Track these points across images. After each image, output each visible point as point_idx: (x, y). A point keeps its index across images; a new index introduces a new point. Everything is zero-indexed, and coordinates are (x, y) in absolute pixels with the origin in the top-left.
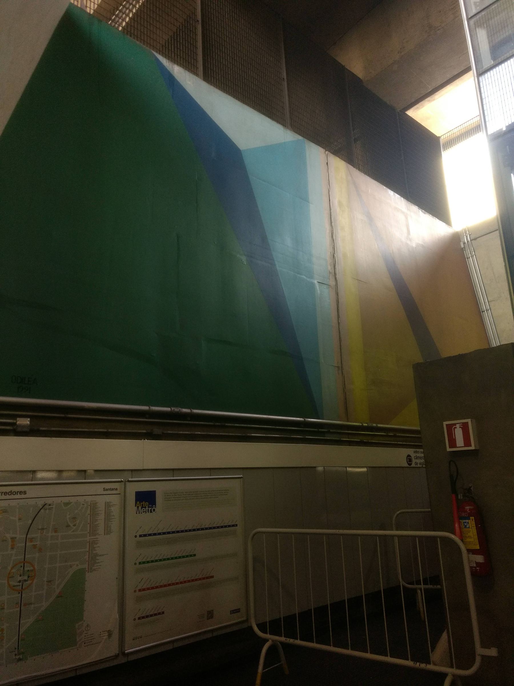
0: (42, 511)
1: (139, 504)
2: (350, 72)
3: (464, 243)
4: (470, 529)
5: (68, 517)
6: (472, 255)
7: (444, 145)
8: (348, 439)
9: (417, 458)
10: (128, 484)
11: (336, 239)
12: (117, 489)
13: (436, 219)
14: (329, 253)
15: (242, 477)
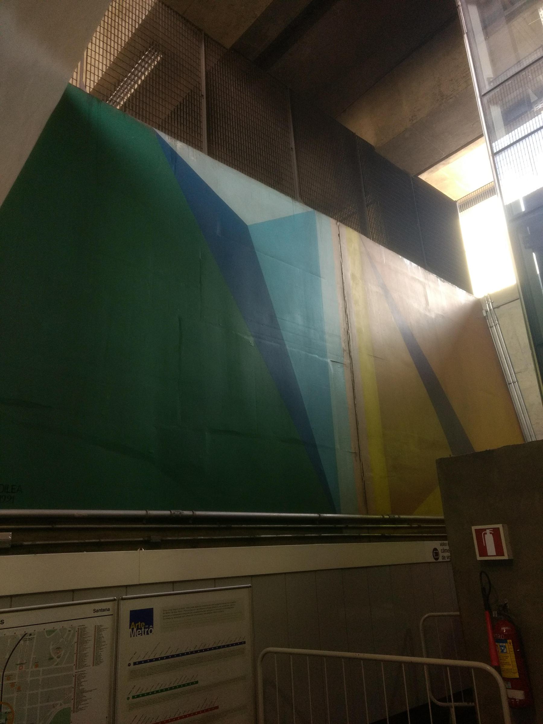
0: (22, 642)
1: (134, 625)
2: (362, 139)
3: (487, 312)
4: (509, 655)
5: (51, 647)
6: (495, 324)
7: (460, 206)
8: (369, 534)
9: (444, 551)
10: (122, 602)
11: (349, 314)
12: (109, 609)
13: (456, 287)
14: (343, 329)
15: (250, 587)
